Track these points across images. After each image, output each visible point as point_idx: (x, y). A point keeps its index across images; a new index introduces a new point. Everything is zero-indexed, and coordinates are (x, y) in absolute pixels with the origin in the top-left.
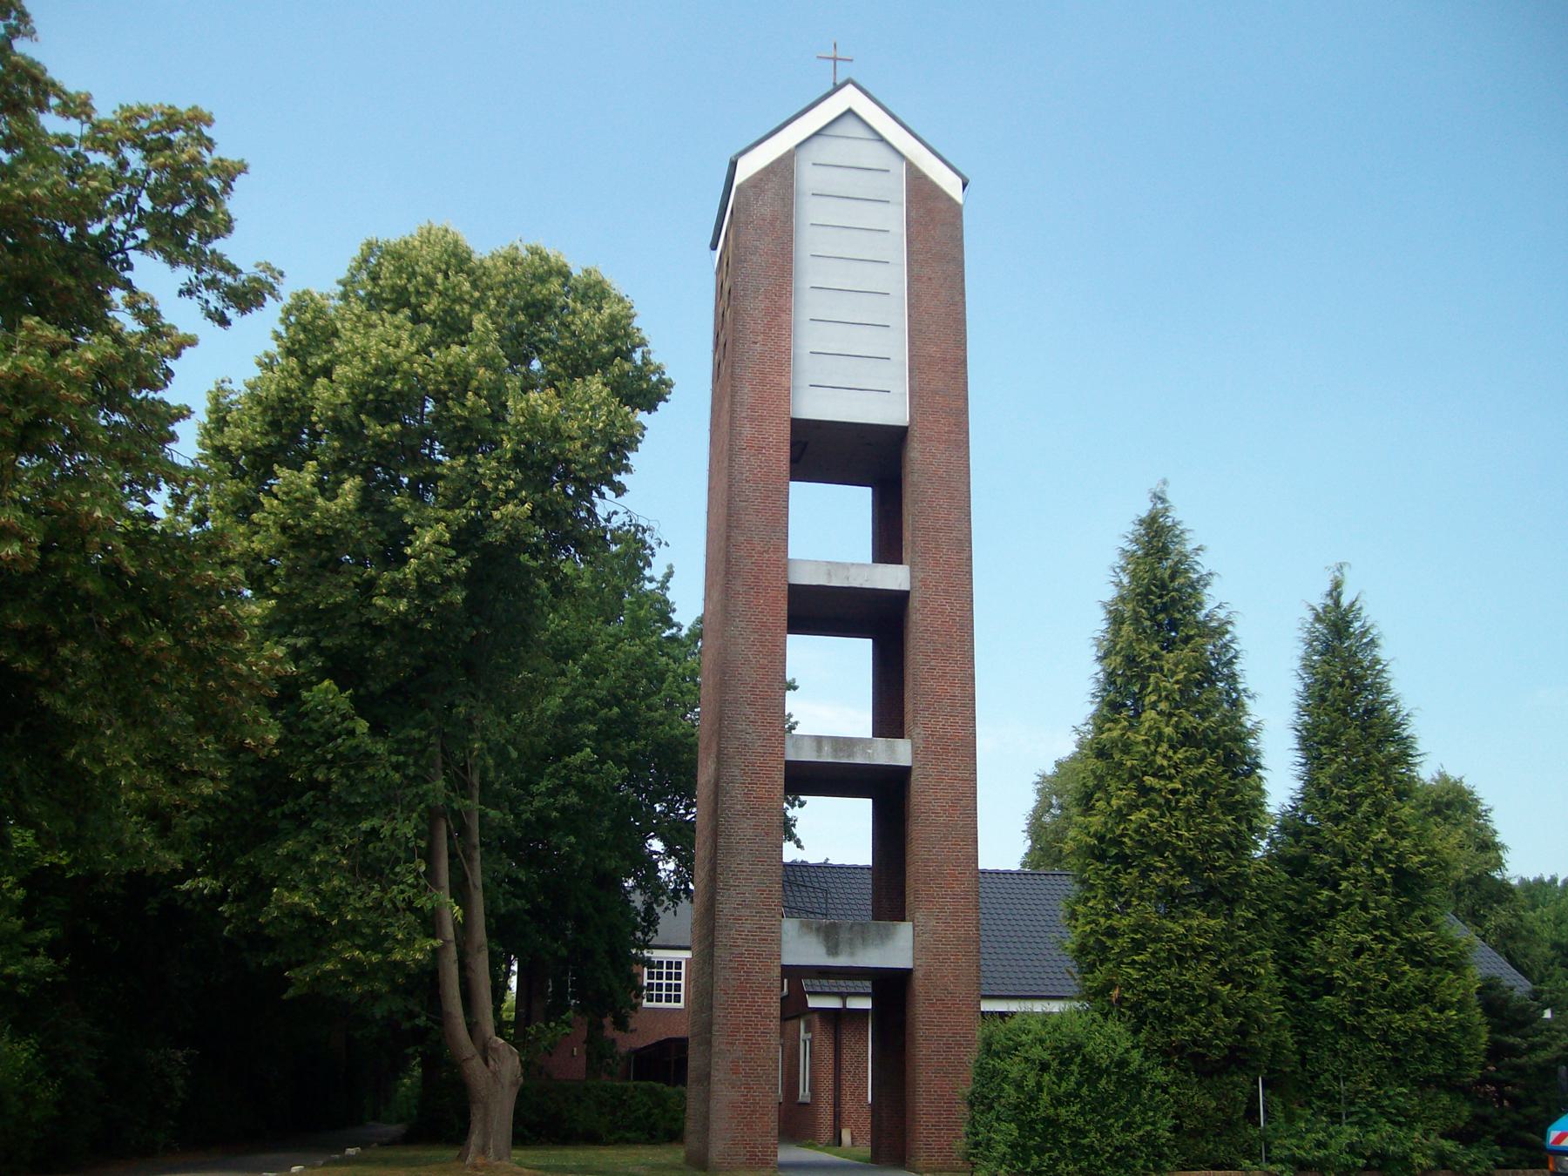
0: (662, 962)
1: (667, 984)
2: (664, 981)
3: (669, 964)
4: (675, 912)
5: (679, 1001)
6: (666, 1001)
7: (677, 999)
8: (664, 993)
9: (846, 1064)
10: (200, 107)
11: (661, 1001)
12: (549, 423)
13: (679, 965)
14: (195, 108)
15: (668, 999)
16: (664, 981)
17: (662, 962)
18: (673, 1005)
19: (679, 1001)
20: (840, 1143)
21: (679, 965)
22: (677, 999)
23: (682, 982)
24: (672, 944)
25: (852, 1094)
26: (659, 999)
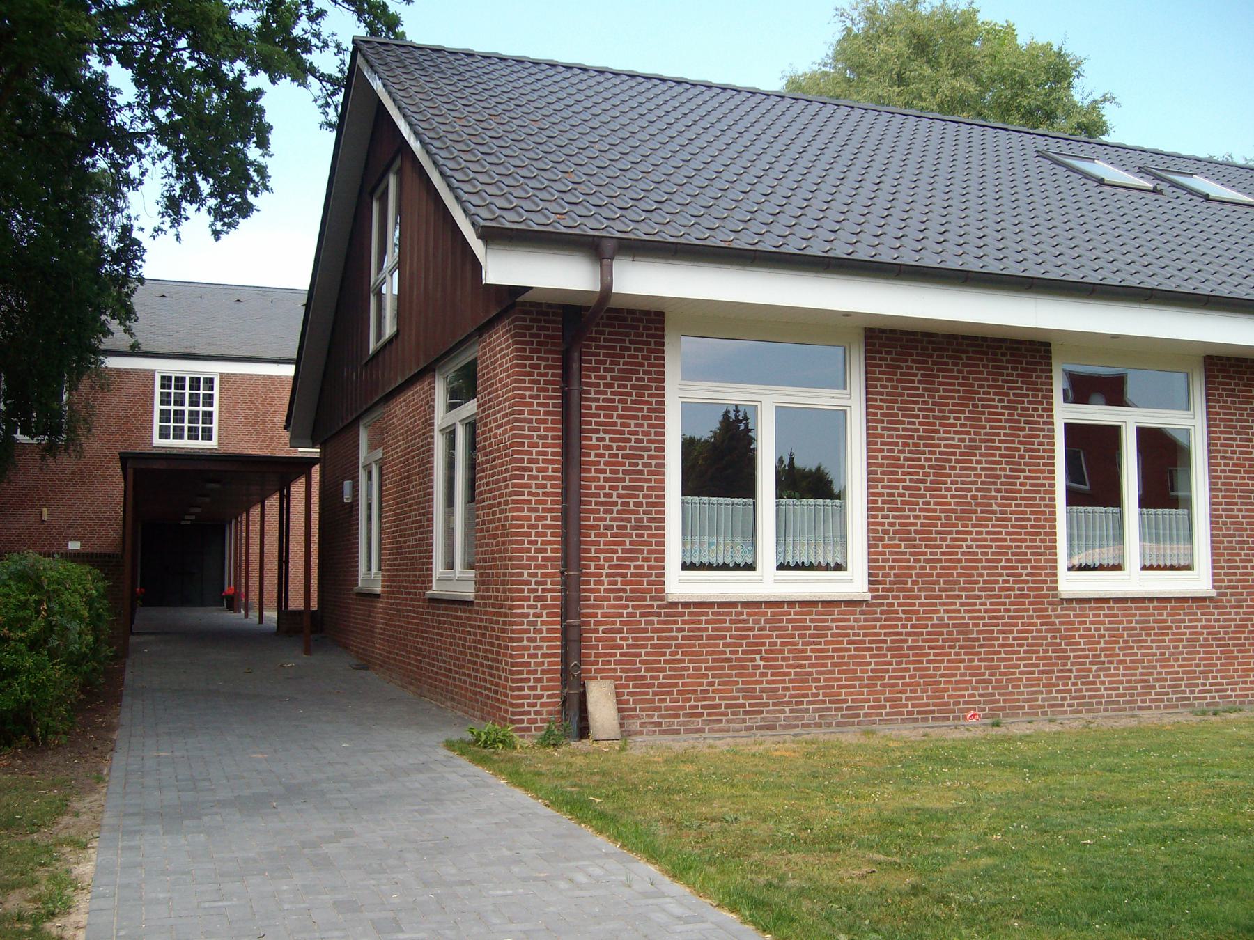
0: (183, 379)
1: (191, 413)
2: (187, 408)
3: (195, 382)
4: (178, 238)
5: (210, 438)
6: (190, 438)
7: (208, 434)
8: (186, 425)
9: (596, 482)
10: (273, 131)
11: (181, 437)
12: (100, 584)
13: (209, 382)
14: (271, 127)
15: (193, 434)
16: (187, 408)
17: (183, 379)
18: (200, 444)
19: (210, 438)
20: (583, 732)
21: (209, 382)
22: (208, 434)
23: (215, 409)
24: (198, 351)
25: (618, 571)
26: (178, 434)
